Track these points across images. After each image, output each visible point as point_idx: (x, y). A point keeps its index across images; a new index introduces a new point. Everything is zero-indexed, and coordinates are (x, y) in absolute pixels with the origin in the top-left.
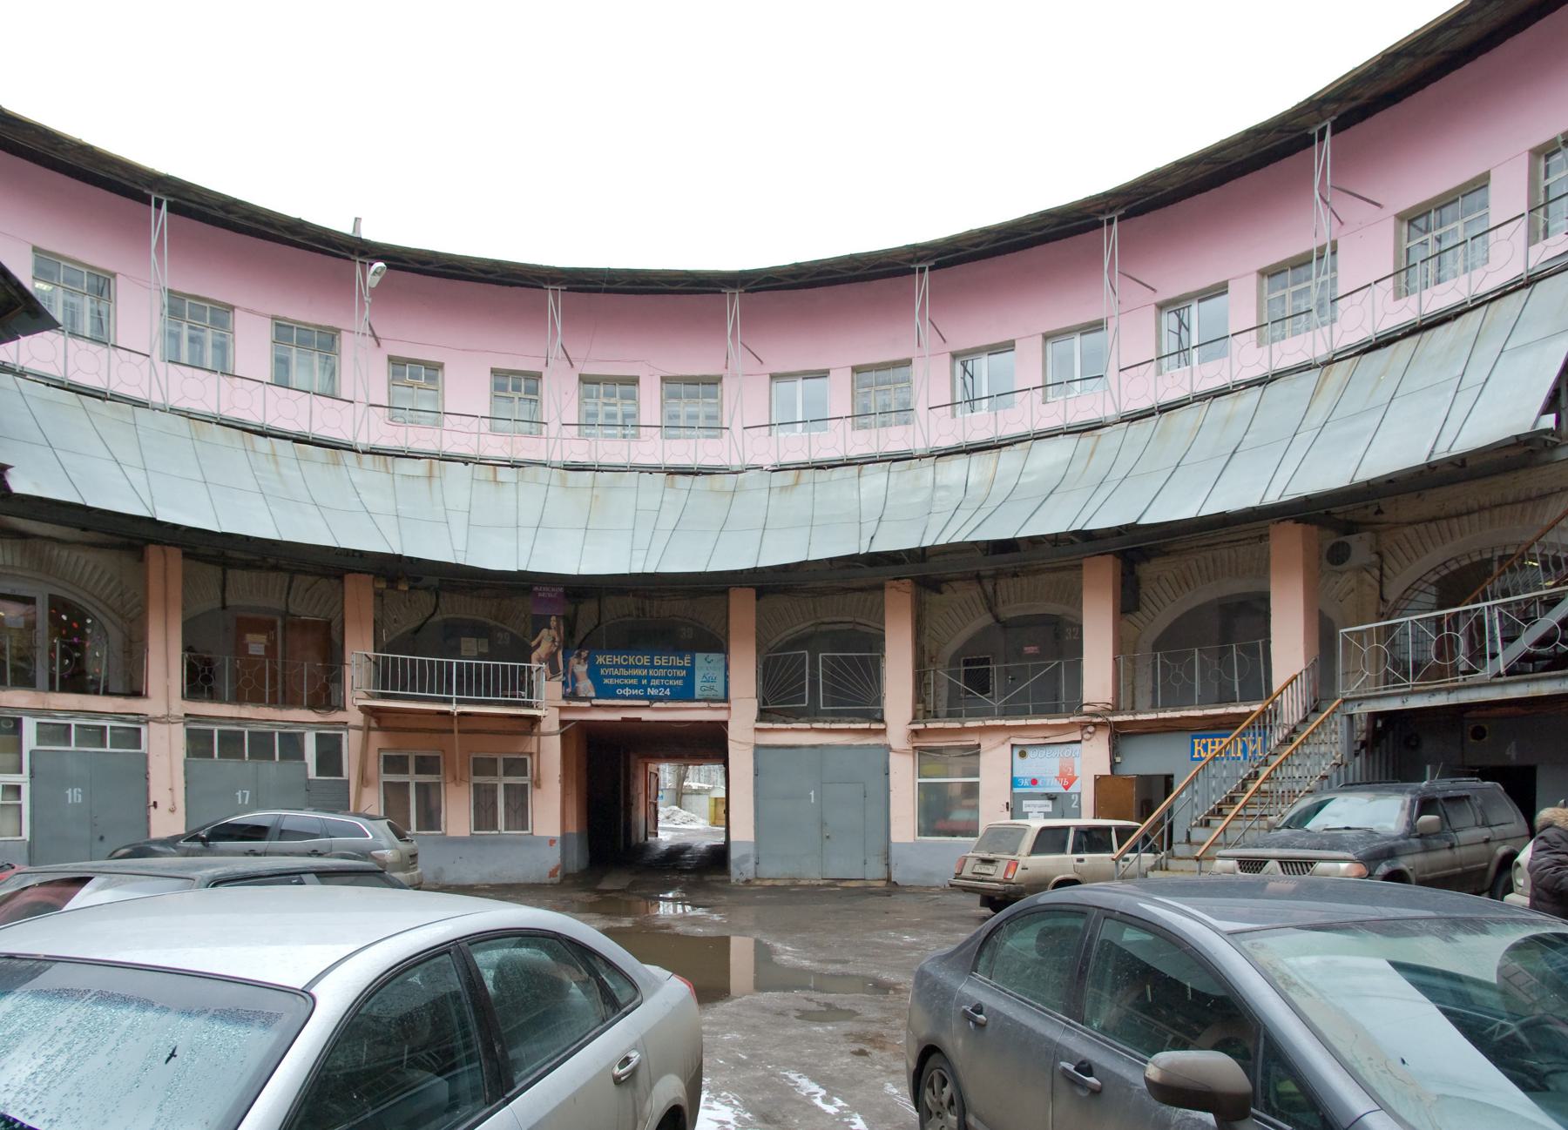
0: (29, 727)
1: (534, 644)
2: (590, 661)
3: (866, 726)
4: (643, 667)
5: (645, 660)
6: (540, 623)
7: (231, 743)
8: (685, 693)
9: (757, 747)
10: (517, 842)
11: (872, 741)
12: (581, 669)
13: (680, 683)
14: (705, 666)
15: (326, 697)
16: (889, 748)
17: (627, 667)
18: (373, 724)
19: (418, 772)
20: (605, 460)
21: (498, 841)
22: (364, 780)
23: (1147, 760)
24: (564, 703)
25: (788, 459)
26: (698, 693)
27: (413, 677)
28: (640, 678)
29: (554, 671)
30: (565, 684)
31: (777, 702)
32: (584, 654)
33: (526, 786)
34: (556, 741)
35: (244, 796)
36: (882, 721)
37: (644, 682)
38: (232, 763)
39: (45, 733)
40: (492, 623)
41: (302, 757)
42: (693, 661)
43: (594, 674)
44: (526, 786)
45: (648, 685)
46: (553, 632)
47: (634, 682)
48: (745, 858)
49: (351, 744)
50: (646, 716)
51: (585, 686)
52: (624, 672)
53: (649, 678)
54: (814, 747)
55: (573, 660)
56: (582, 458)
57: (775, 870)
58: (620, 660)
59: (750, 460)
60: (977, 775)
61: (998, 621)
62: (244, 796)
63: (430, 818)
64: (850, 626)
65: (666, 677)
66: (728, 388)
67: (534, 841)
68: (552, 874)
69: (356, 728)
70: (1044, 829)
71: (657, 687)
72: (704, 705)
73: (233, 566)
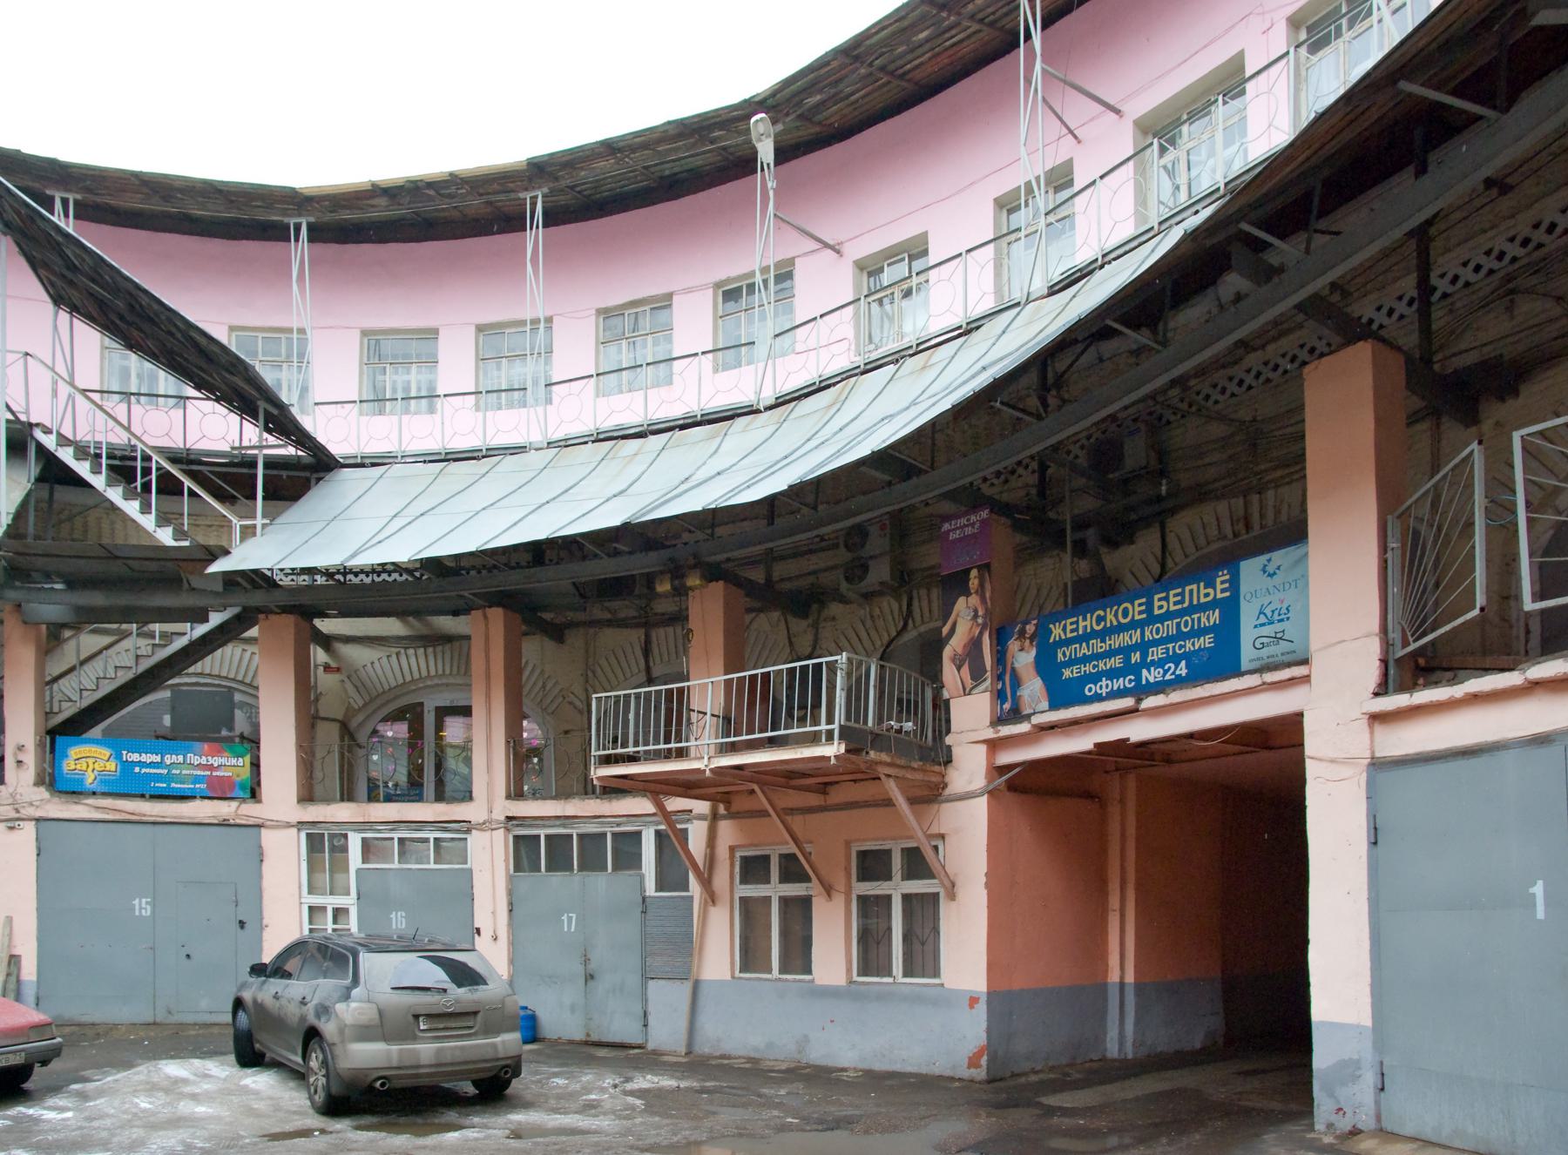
0: (355, 842)
1: (945, 630)
4: (1133, 625)
5: (1136, 610)
7: (558, 845)
8: (1220, 662)
9: (1378, 765)
10: (917, 999)
12: (1024, 658)
13: (1206, 641)
17: (1102, 635)
18: (722, 809)
21: (883, 997)
24: (990, 734)
27: (657, 708)
28: (1125, 651)
29: (977, 675)
30: (1000, 696)
32: (1030, 628)
33: (936, 896)
34: (979, 809)
35: (570, 919)
37: (1136, 657)
38: (558, 877)
39: (366, 845)
42: (1234, 585)
43: (1047, 667)
44: (936, 896)
46: (974, 600)
47: (1116, 662)
48: (1348, 1070)
50: (1138, 731)
51: (1033, 689)
52: (1098, 646)
53: (1144, 646)
55: (1013, 645)
58: (1087, 623)
62: (570, 919)
63: (798, 955)
65: (1180, 636)
67: (944, 999)
68: (973, 1062)
69: (701, 817)
70: (1282, 237)
71: (1159, 664)
73: (657, 625)
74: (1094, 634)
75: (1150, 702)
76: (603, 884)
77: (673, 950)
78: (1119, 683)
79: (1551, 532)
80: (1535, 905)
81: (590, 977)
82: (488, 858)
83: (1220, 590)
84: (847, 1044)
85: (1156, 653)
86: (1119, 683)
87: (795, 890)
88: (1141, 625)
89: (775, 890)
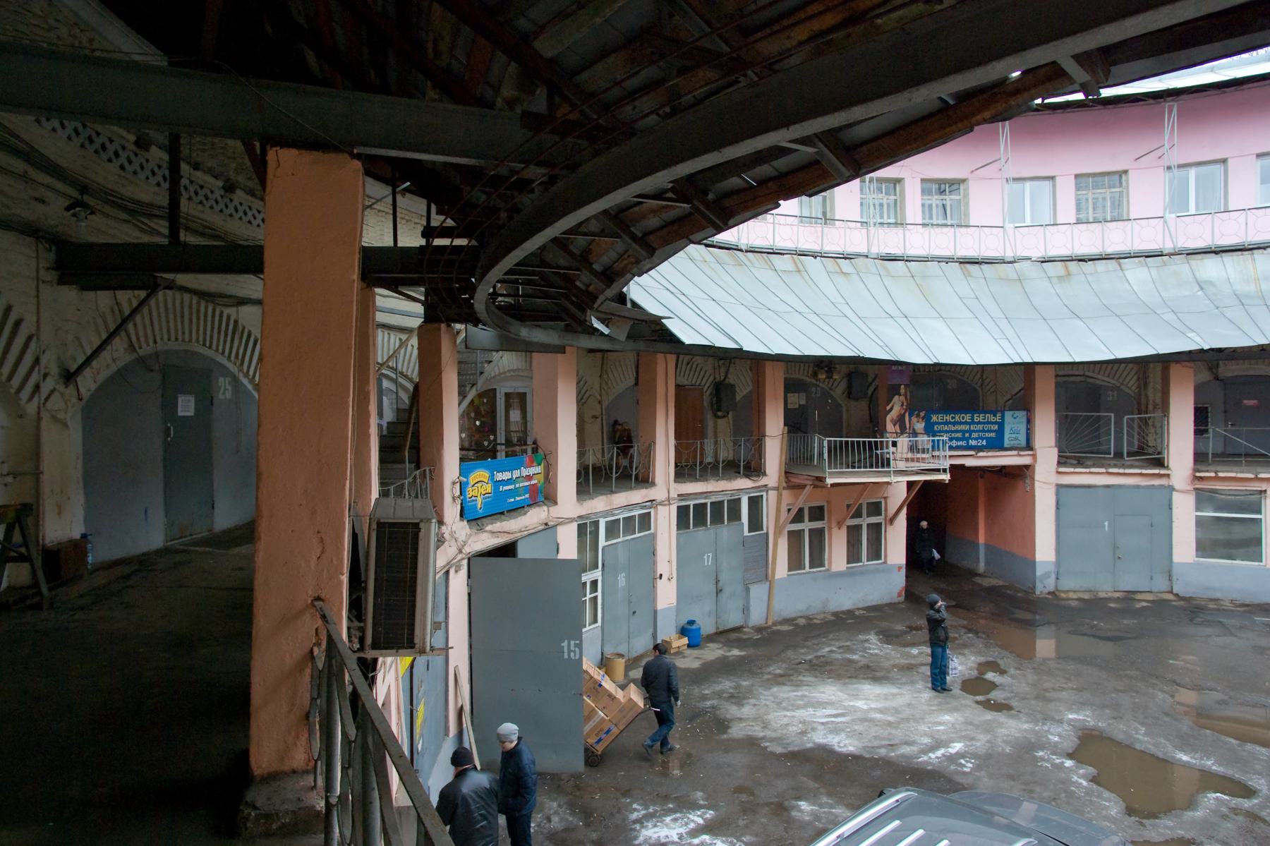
2: (927, 419)
3: (1156, 471)
4: (966, 423)
5: (967, 418)
6: (894, 390)
8: (997, 444)
11: (1157, 482)
13: (993, 435)
14: (1014, 424)
15: (754, 468)
16: (1172, 488)
17: (954, 424)
19: (810, 520)
20: (912, 252)
24: (910, 455)
25: (1052, 253)
26: (1007, 443)
28: (964, 432)
31: (1075, 450)
32: (922, 414)
36: (1167, 468)
40: (808, 380)
41: (740, 519)
44: (880, 524)
45: (970, 438)
46: (902, 398)
47: (959, 435)
48: (1047, 575)
49: (770, 504)
53: (970, 432)
54: (1108, 486)
56: (897, 251)
57: (1075, 584)
58: (949, 418)
59: (1021, 253)
60: (1259, 512)
61: (1217, 378)
63: (818, 559)
64: (1082, 379)
65: (983, 431)
68: (899, 595)
72: (1015, 452)
74: (950, 423)
75: (981, 454)
76: (725, 532)
77: (759, 566)
78: (960, 443)
79: (725, 237)
80: (383, 450)
81: (719, 591)
82: (665, 521)
83: (998, 419)
84: (848, 598)
85: (975, 435)
86: (960, 443)
87: (817, 525)
88: (969, 424)
89: (806, 526)
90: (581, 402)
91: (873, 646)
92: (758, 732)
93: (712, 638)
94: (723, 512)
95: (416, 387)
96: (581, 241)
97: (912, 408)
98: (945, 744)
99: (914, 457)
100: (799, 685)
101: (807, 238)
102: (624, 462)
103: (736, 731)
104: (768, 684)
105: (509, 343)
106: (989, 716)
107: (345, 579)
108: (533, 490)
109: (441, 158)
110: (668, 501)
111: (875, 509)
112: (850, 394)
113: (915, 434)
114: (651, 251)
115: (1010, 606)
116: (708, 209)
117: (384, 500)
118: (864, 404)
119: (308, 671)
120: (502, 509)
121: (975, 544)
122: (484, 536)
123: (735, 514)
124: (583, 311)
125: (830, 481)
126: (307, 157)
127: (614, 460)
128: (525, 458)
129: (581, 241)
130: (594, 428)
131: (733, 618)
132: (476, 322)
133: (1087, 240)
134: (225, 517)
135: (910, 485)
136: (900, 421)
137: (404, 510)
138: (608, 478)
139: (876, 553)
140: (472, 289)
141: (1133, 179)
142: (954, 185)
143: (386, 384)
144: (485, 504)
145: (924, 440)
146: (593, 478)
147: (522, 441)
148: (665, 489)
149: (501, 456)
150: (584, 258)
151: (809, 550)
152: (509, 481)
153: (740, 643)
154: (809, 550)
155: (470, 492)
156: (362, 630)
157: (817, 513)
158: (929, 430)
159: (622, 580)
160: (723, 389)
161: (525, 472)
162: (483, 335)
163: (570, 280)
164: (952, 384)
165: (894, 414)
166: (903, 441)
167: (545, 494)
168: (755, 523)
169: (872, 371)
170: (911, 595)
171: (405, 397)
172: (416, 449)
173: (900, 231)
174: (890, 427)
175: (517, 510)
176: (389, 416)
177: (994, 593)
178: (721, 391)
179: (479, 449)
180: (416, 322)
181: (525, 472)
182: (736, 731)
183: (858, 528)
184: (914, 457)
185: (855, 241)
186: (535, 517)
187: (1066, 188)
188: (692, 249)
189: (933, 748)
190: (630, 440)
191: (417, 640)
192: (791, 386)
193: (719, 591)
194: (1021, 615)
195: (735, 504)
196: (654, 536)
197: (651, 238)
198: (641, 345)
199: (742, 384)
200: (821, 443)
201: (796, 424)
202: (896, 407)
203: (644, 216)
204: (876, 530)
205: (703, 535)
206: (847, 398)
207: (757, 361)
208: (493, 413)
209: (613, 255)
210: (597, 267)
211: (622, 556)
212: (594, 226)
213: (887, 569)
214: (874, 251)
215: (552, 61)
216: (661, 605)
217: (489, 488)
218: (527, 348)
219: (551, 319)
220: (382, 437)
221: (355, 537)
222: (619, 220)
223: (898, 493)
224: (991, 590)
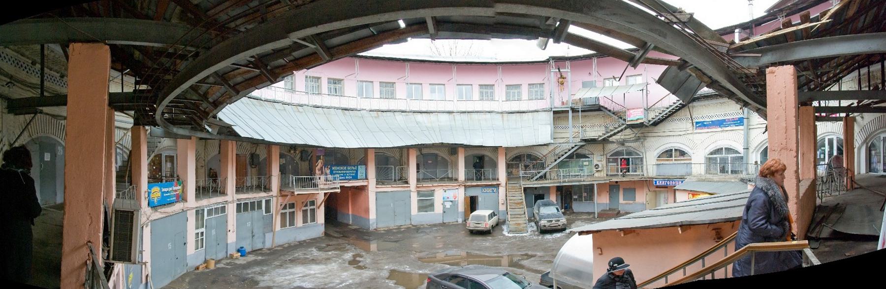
2: (331, 168)
6: (319, 158)
8: (355, 178)
14: (361, 170)
15: (267, 189)
20: (325, 105)
22: (277, 214)
23: (473, 192)
25: (373, 108)
57: (382, 226)
63: (292, 223)
66: (496, 87)
76: (256, 213)
77: (269, 226)
79: (256, 93)
80: (117, 177)
81: (253, 236)
82: (231, 209)
84: (303, 236)
87: (291, 210)
89: (288, 211)
90: (197, 161)
91: (315, 252)
92: (271, 284)
93: (249, 253)
94: (254, 206)
95: (131, 152)
96: (204, 87)
97: (325, 165)
98: (346, 281)
99: (326, 184)
100: (286, 268)
101: (286, 97)
102: (214, 185)
103: (262, 285)
104: (274, 269)
105: (168, 135)
106: (359, 271)
107: (101, 235)
108: (178, 196)
109: (156, 45)
110: (233, 202)
111: (313, 203)
112: (302, 159)
113: (326, 174)
114: (238, 92)
115: (362, 235)
116: (269, 71)
117: (118, 200)
118: (307, 163)
119: (85, 269)
120: (164, 203)
121: (348, 214)
122: (157, 213)
123: (260, 207)
124: (202, 120)
125: (296, 193)
126: (86, 45)
127: (211, 183)
128: (174, 183)
129: (204, 87)
130: (202, 171)
131: (259, 246)
132: (154, 124)
133: (384, 105)
134: (59, 200)
135: (325, 194)
136: (321, 169)
137: (126, 205)
138: (208, 192)
139: (313, 219)
140: (154, 110)
141: (397, 85)
142: (339, 81)
143: (118, 150)
144: (158, 201)
145: (330, 177)
146: (201, 191)
147: (172, 176)
148: (232, 196)
149: (164, 181)
150: (205, 96)
151: (288, 220)
152: (168, 192)
153: (262, 255)
154: (288, 220)
155: (152, 196)
156: (109, 252)
157: (292, 206)
158: (332, 173)
159: (213, 232)
160: (256, 158)
161: (175, 188)
162: (158, 130)
163: (197, 106)
164: (339, 155)
165: (319, 167)
166: (323, 177)
167: (182, 198)
168: (268, 210)
169: (310, 150)
170: (326, 234)
171: (126, 157)
172: (130, 177)
173: (320, 96)
174: (317, 172)
175: (171, 204)
176: (120, 163)
177: (356, 231)
178: (253, 156)
179: (155, 178)
180: (130, 126)
181: (175, 188)
182: (262, 285)
183: (306, 210)
184: (326, 184)
185: (303, 99)
186: (178, 207)
187: (377, 86)
188: (244, 99)
189: (341, 284)
190: (216, 176)
191: (132, 259)
192: (282, 156)
193: (253, 236)
194: (366, 237)
195: (260, 203)
196: (227, 215)
197: (237, 87)
198: (223, 137)
199: (262, 153)
200: (292, 178)
201: (283, 170)
202: (320, 163)
203: (235, 76)
204: (313, 211)
205: (247, 215)
206: (302, 160)
207: (269, 145)
208: (160, 163)
209: (218, 94)
210: (211, 100)
211: (214, 223)
212: (211, 80)
213: (317, 225)
214: (311, 104)
215: (197, 5)
216: (229, 241)
217: (159, 194)
218: (175, 137)
219: (185, 124)
220: (117, 172)
221: (106, 213)
222: (223, 78)
223: (321, 198)
224: (355, 230)
